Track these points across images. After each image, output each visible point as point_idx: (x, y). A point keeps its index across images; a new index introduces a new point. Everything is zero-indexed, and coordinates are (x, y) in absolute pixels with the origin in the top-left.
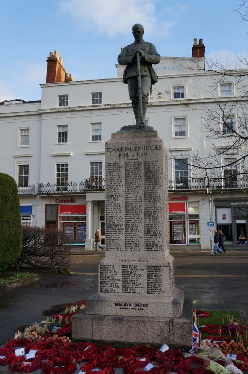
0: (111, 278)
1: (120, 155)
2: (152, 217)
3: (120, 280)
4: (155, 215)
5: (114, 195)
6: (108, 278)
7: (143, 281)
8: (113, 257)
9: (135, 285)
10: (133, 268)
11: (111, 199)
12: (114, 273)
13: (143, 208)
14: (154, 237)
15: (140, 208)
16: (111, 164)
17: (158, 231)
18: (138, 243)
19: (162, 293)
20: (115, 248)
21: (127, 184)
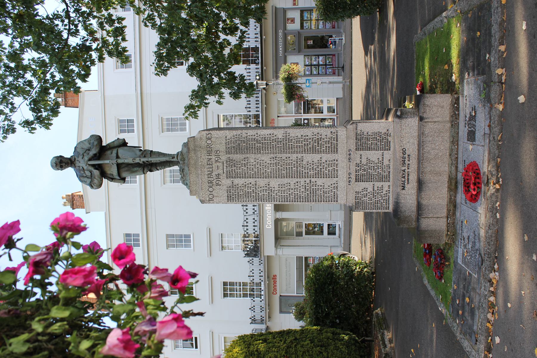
1: (218, 185)
4: (294, 141)
7: (374, 155)
12: (364, 192)
13: (284, 156)
14: (320, 142)
18: (328, 162)
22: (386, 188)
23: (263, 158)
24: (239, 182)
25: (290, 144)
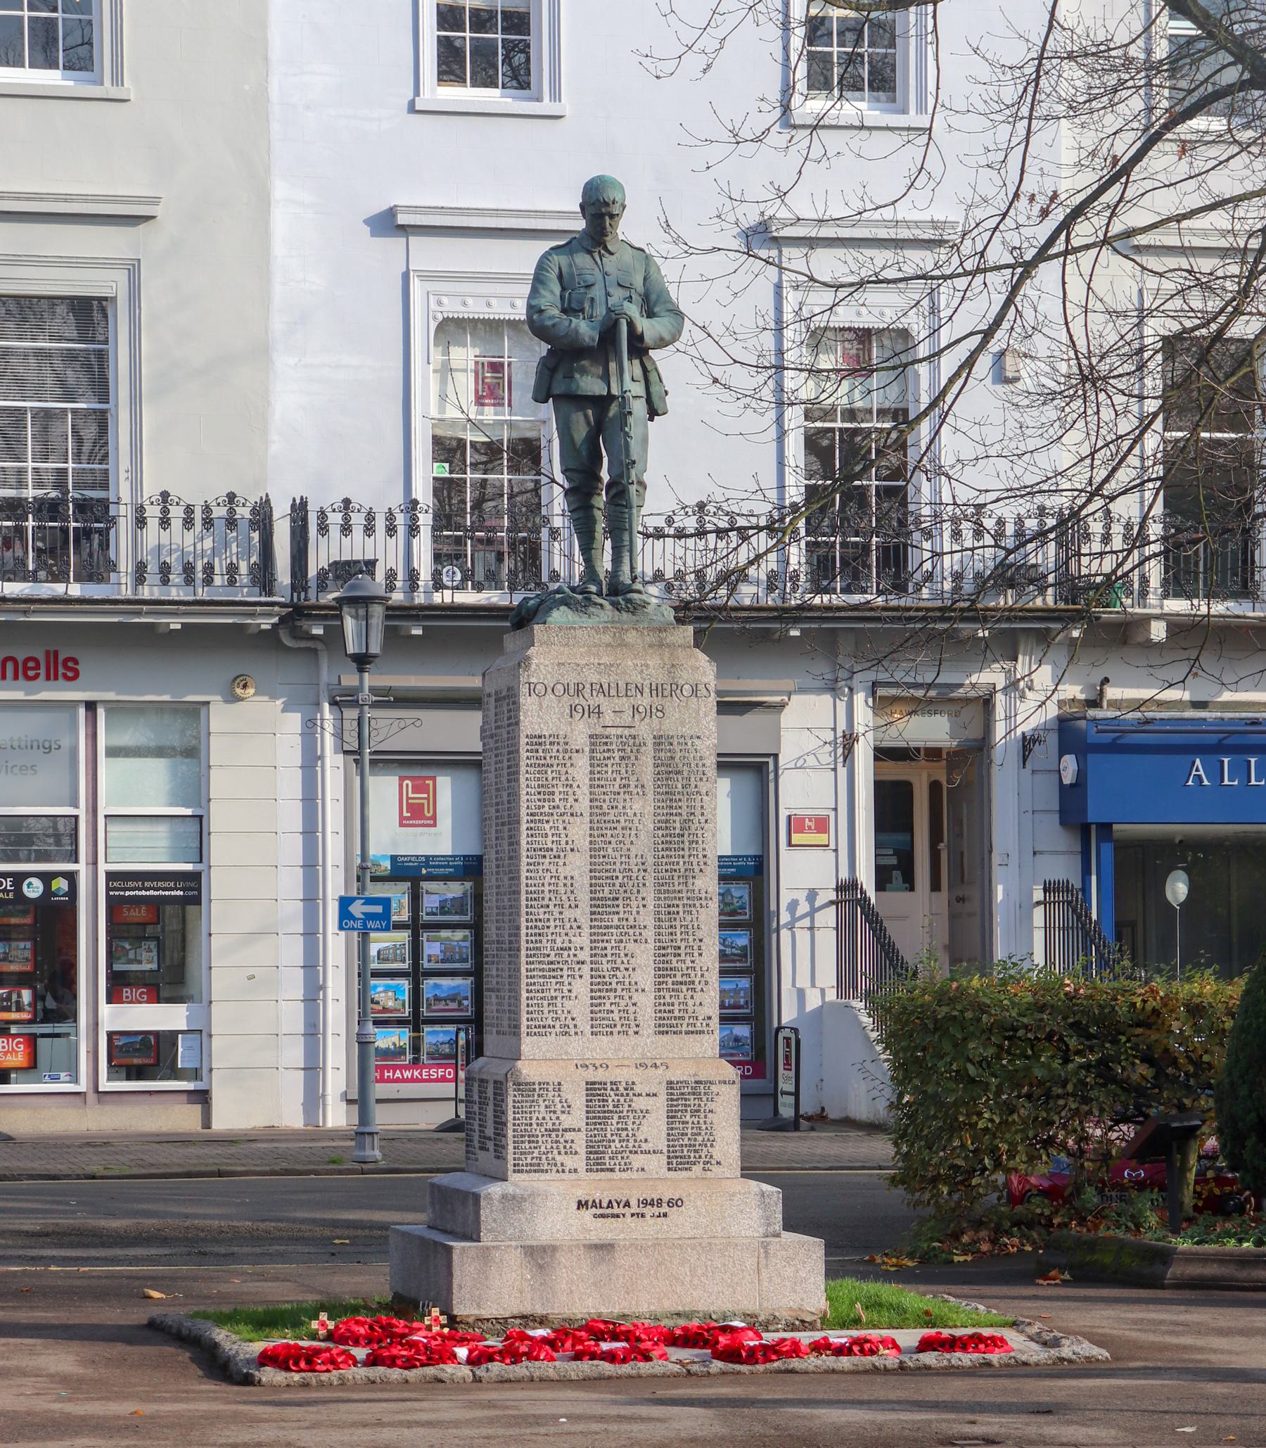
0: (550, 1124)
1: (573, 709)
2: (678, 923)
3: (579, 1130)
4: (689, 918)
5: (554, 846)
6: (541, 1125)
7: (654, 1130)
8: (548, 1055)
9: (630, 1145)
10: (621, 1089)
11: (541, 861)
12: (559, 1106)
14: (684, 988)
15: (638, 892)
16: (540, 737)
17: (698, 969)
18: (631, 1009)
19: (715, 1168)
20: (557, 1024)
21: (598, 811)
22: (570, 1162)
23: (643, 835)
24: (581, 769)
25: (681, 909)
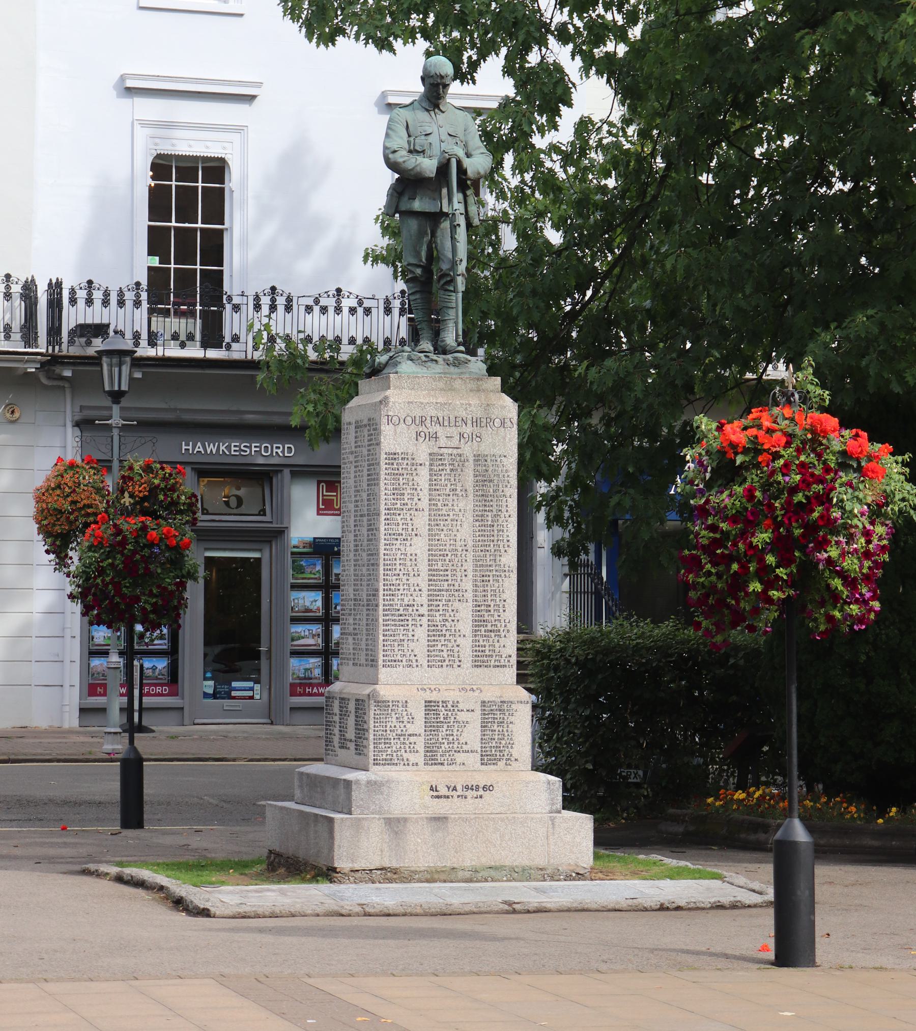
1: (418, 434)
7: (472, 735)
12: (406, 718)
13: (469, 566)
14: (493, 634)
18: (456, 649)
22: (413, 758)
23: (465, 525)
